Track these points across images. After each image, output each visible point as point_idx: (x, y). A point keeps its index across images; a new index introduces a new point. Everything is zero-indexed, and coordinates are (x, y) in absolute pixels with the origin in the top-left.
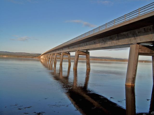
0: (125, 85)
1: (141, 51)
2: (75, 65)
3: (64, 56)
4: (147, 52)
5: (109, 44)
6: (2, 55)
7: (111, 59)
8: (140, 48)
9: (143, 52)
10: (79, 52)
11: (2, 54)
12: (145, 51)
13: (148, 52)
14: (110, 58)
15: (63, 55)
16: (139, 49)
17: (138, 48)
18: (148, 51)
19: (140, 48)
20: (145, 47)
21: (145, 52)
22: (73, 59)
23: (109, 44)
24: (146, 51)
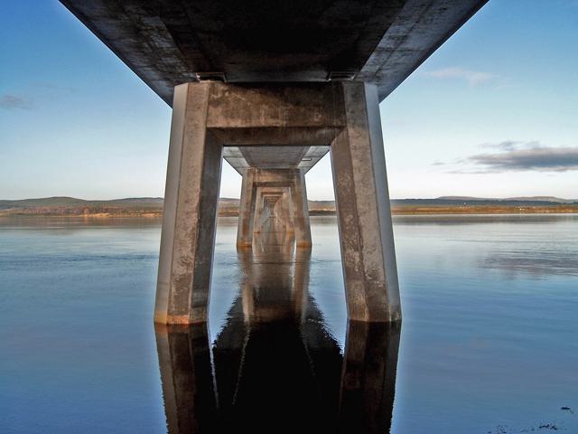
0: (155, 323)
1: (226, 117)
2: (241, 232)
3: (259, 191)
4: (263, 122)
5: (352, 112)
6: (142, 211)
7: (554, 203)
8: (213, 103)
9: (237, 123)
10: (254, 174)
11: (141, 208)
12: (255, 113)
13: (272, 122)
14: (552, 200)
15: (255, 186)
16: (211, 108)
17: (205, 100)
18: (273, 117)
19: (213, 103)
20: (251, 93)
21: (254, 124)
22: (448, 211)
23: (352, 112)
24: (259, 117)
